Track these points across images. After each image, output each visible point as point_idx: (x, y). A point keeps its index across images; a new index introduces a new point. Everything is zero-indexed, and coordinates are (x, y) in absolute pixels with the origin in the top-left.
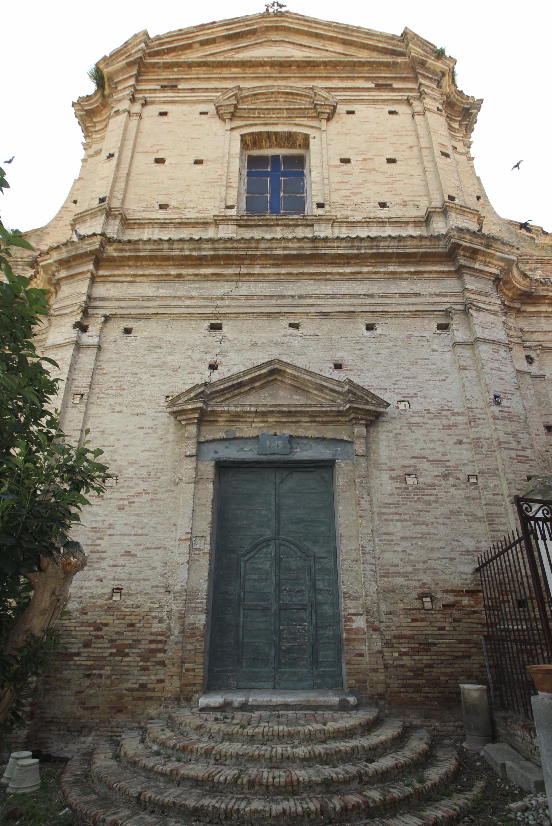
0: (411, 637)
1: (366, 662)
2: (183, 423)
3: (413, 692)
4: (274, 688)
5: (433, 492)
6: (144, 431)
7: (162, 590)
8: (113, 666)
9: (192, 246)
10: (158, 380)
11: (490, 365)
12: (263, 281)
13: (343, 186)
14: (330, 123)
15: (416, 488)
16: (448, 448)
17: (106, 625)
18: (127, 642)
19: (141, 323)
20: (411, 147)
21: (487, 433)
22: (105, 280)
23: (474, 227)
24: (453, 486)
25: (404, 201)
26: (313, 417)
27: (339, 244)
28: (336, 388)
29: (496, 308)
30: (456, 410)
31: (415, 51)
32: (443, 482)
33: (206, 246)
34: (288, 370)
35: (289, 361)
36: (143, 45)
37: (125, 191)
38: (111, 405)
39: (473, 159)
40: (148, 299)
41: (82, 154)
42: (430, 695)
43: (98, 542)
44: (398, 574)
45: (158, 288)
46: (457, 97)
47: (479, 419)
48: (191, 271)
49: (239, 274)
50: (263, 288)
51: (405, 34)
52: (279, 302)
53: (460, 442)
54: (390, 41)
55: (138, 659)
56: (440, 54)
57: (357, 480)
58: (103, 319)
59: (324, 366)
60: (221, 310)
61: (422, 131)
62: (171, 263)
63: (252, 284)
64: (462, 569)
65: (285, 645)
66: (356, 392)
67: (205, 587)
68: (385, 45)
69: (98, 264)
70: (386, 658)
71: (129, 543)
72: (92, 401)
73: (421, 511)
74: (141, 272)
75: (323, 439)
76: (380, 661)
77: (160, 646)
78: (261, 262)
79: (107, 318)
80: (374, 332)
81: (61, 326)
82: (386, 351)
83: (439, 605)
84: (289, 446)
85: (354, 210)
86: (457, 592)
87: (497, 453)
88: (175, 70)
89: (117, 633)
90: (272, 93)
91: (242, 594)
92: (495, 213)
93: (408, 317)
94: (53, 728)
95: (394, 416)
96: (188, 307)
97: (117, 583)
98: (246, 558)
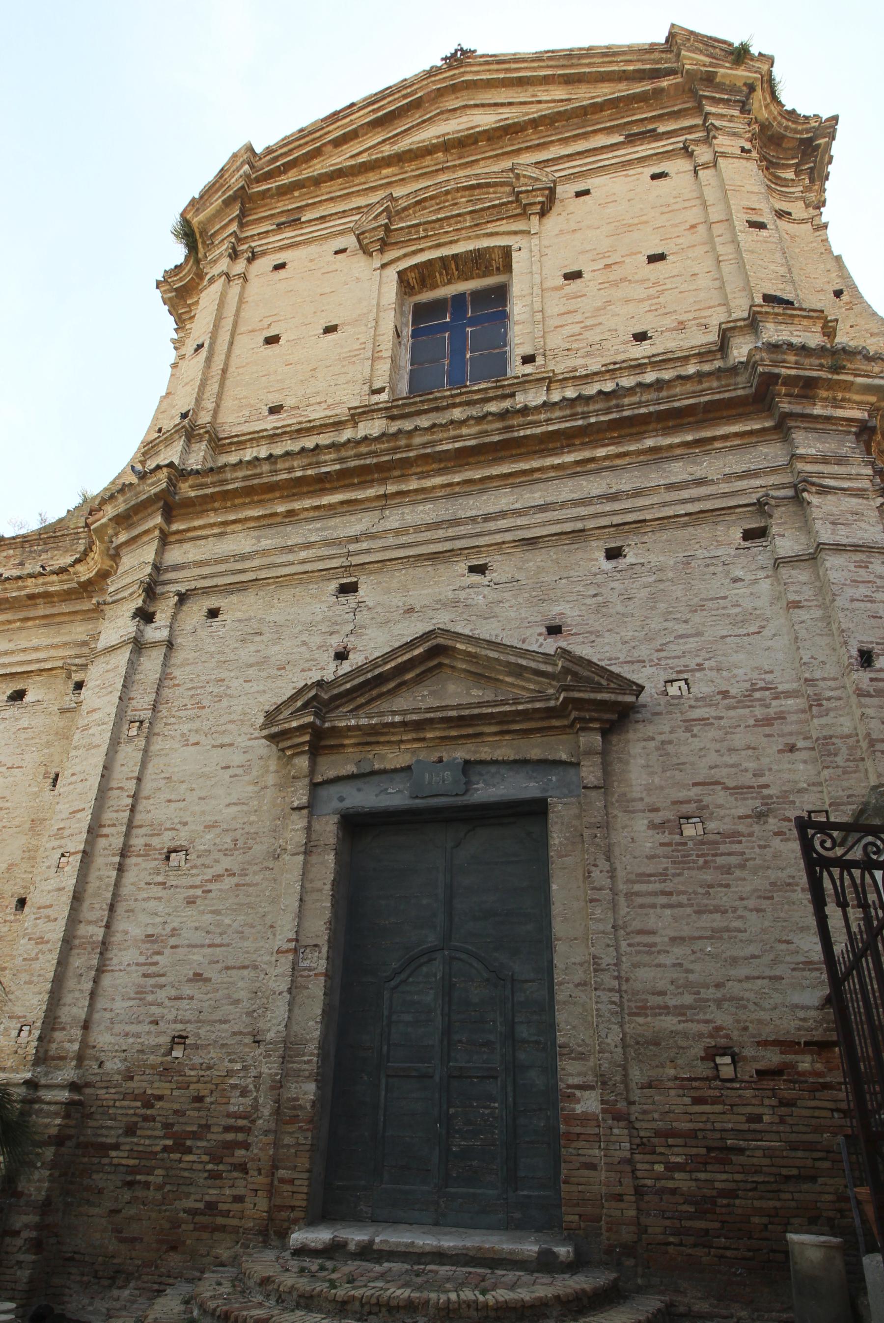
0: (692, 1134)
1: (600, 1181)
2: (289, 753)
3: (695, 1245)
4: (436, 1224)
5: (736, 847)
6: (230, 772)
7: (248, 1040)
8: (167, 1169)
9: (306, 461)
10: (255, 687)
11: (850, 592)
12: (425, 500)
13: (569, 319)
14: (545, 220)
15: (702, 843)
16: (765, 761)
17: (160, 1098)
18: (189, 1129)
19: (234, 598)
20: (693, 227)
21: (845, 724)
22: (183, 538)
23: (814, 339)
24: (776, 834)
25: (681, 323)
26: (506, 723)
27: (549, 415)
28: (543, 667)
29: (866, 484)
30: (781, 688)
31: (693, 60)
32: (756, 828)
33: (327, 457)
34: (458, 646)
35: (467, 632)
36: (246, 167)
37: (220, 396)
38: (183, 735)
39: (825, 226)
40: (243, 557)
41: (171, 355)
42: (728, 1253)
43: (156, 958)
44: (666, 1009)
45: (258, 539)
46: (785, 123)
47: (829, 699)
48: (307, 503)
49: (385, 496)
50: (426, 512)
51: (671, 36)
52: (451, 532)
53: (792, 748)
54: (647, 56)
55: (205, 1158)
56: (740, 55)
57: (587, 833)
58: (176, 598)
59: (528, 632)
60: (355, 560)
61: (711, 194)
62: (277, 494)
63: (407, 510)
64: (798, 998)
65: (458, 1144)
66: (577, 671)
67: (317, 1034)
68: (639, 66)
69: (169, 514)
70: (639, 1174)
71: (201, 959)
72: (156, 730)
73: (711, 886)
74: (232, 517)
75: (524, 762)
76: (627, 1181)
77: (240, 1137)
78: (419, 470)
79: (183, 598)
80: (621, 560)
81: (117, 617)
82: (644, 593)
83: (748, 1071)
84: (464, 780)
85: (588, 355)
86: (786, 1045)
87: (869, 763)
88: (296, 194)
89: (176, 1112)
90: (447, 192)
91: (385, 1048)
92: (874, 314)
93: (685, 525)
94: (74, 1270)
95: (658, 709)
96: (303, 562)
97: (180, 1026)
98: (393, 983)
